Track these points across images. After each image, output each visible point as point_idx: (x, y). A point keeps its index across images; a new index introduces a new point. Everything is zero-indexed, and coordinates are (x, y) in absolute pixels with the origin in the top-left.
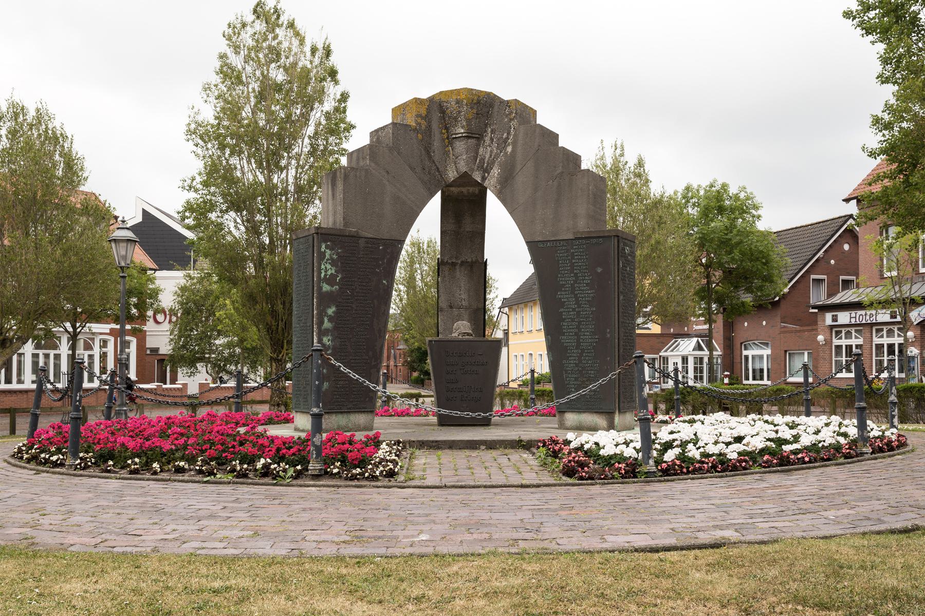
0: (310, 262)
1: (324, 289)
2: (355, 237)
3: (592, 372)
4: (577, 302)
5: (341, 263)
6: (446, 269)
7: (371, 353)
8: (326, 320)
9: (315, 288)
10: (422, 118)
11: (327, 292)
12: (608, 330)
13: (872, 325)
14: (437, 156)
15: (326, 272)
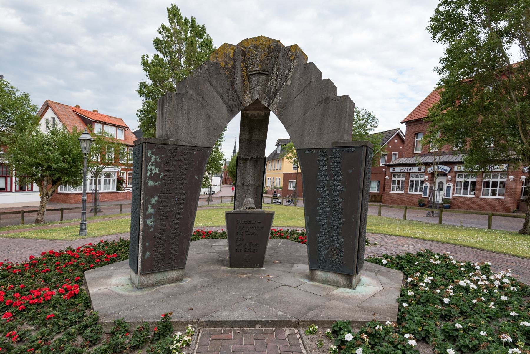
0: (140, 164)
1: (149, 185)
3: (338, 245)
6: (241, 163)
7: (183, 228)
8: (150, 207)
9: (143, 184)
10: (231, 59)
11: (151, 186)
12: (353, 216)
13: (409, 173)
14: (238, 87)
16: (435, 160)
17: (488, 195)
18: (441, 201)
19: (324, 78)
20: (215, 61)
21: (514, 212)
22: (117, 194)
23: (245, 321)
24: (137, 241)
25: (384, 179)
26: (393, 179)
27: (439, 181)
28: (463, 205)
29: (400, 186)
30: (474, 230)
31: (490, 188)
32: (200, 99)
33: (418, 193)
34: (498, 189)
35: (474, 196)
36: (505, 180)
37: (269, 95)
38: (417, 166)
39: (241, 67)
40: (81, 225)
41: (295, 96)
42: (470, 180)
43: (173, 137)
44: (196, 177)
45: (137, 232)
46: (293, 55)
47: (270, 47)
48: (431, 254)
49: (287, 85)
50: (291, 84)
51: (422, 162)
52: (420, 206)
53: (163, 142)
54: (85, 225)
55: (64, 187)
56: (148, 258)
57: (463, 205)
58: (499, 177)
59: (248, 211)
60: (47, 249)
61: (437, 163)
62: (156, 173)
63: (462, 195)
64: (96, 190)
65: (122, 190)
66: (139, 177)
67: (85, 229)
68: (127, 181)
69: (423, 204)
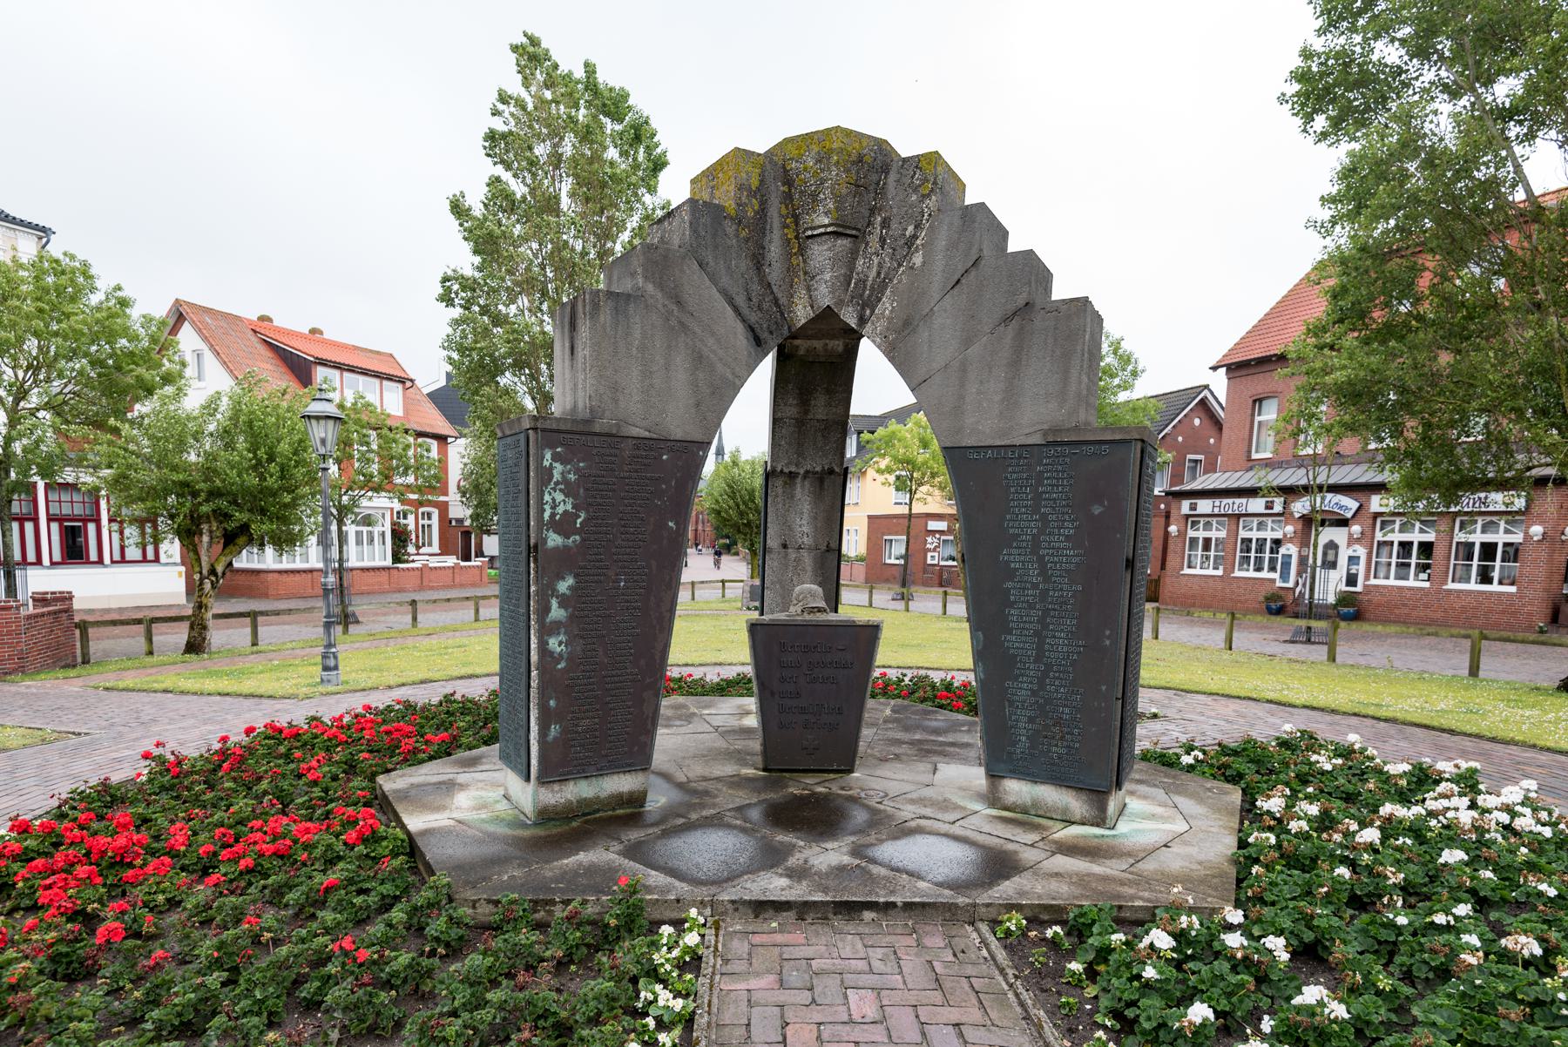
0: (522, 487)
1: (550, 544)
2: (613, 438)
3: (1067, 710)
4: (1043, 571)
5: (586, 491)
6: (778, 483)
7: (642, 662)
8: (554, 603)
10: (752, 194)
11: (556, 549)
12: (1108, 633)
13: (1239, 516)
14: (775, 273)
15: (554, 507)
16: (1315, 478)
17: (1468, 581)
18: (1331, 599)
19: (1013, 246)
20: (706, 197)
21: (1542, 631)
22: (395, 572)
23: (833, 902)
24: (523, 695)
25: (1162, 533)
26: (1191, 533)
27: (1326, 541)
28: (1396, 611)
29: (1212, 553)
30: (1432, 680)
31: (1475, 562)
32: (674, 307)
33: (1265, 574)
34: (1498, 563)
35: (1427, 585)
36: (1517, 538)
37: (862, 295)
38: (1263, 496)
39: (781, 216)
40: (325, 656)
41: (937, 297)
42: (1416, 537)
43: (607, 414)
44: (670, 524)
45: (523, 670)
46: (928, 181)
47: (860, 159)
48: (1311, 741)
49: (912, 268)
50: (924, 263)
51: (1275, 484)
52: (1271, 612)
53: (581, 428)
54: (336, 658)
55: (255, 550)
56: (555, 739)
57: (1396, 611)
58: (1502, 529)
59: (807, 617)
60: (259, 717)
61: (1320, 488)
62: (566, 512)
63: (1392, 582)
64: (341, 560)
65: (407, 562)
66: (523, 521)
67: (336, 668)
68: (417, 537)
69: (1277, 606)
